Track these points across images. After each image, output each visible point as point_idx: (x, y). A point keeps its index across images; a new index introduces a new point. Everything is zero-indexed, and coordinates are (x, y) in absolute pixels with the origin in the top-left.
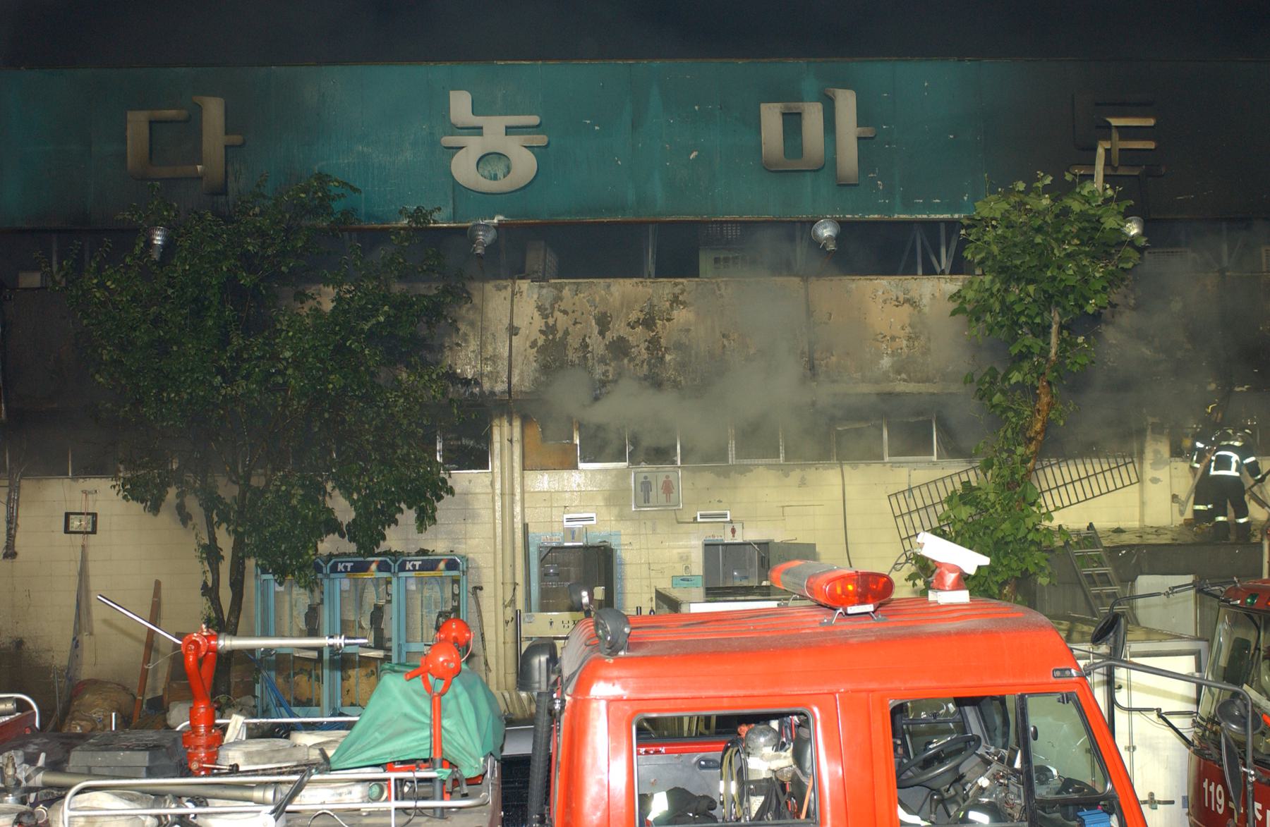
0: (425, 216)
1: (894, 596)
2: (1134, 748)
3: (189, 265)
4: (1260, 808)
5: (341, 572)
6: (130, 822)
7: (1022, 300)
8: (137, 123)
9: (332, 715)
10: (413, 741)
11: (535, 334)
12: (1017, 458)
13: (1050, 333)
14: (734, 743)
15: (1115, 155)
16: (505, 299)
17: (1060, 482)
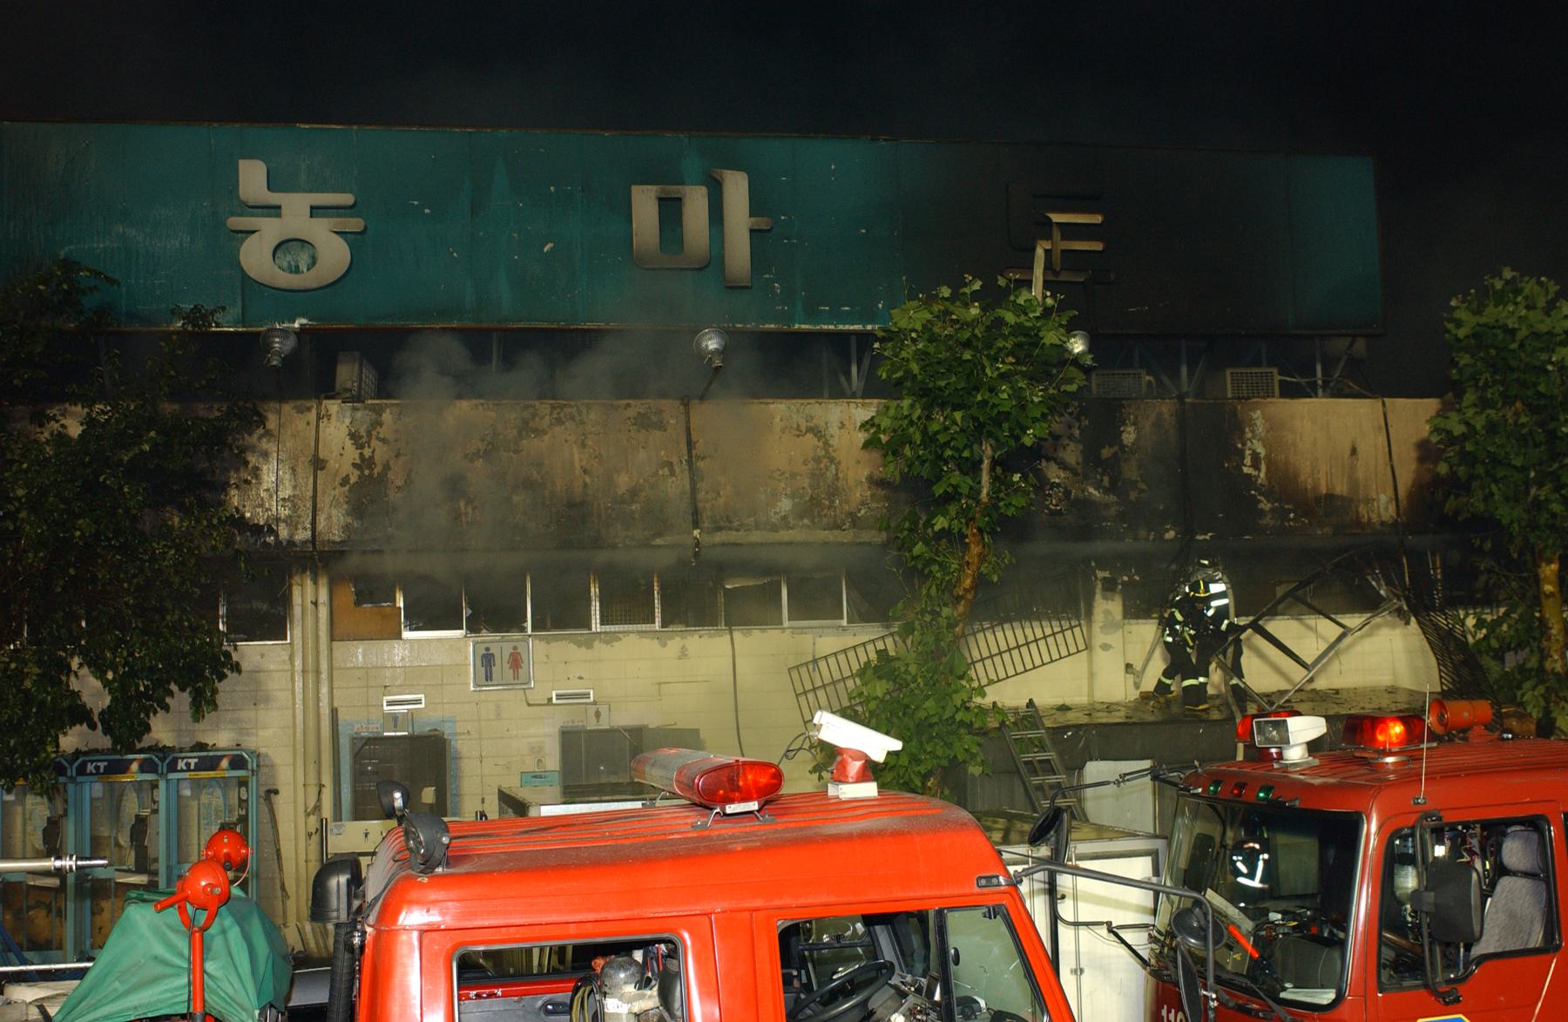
0: (204, 317)
1: (785, 790)
2: (1082, 971)
5: (91, 774)
7: (946, 429)
9: (79, 961)
10: (166, 991)
11: (346, 469)
12: (943, 622)
13: (981, 470)
14: (587, 981)
15: (1057, 258)
17: (1003, 647)
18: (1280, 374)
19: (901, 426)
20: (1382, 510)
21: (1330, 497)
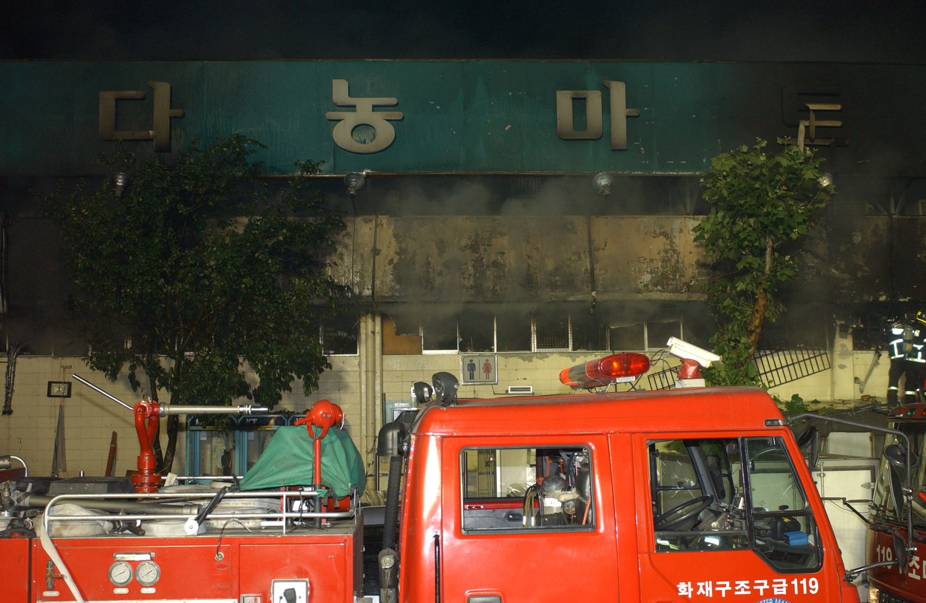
3: (142, 198)
4: (918, 560)
6: (93, 527)
8: (107, 99)
11: (392, 254)
13: (765, 254)
16: (370, 229)
17: (778, 366)
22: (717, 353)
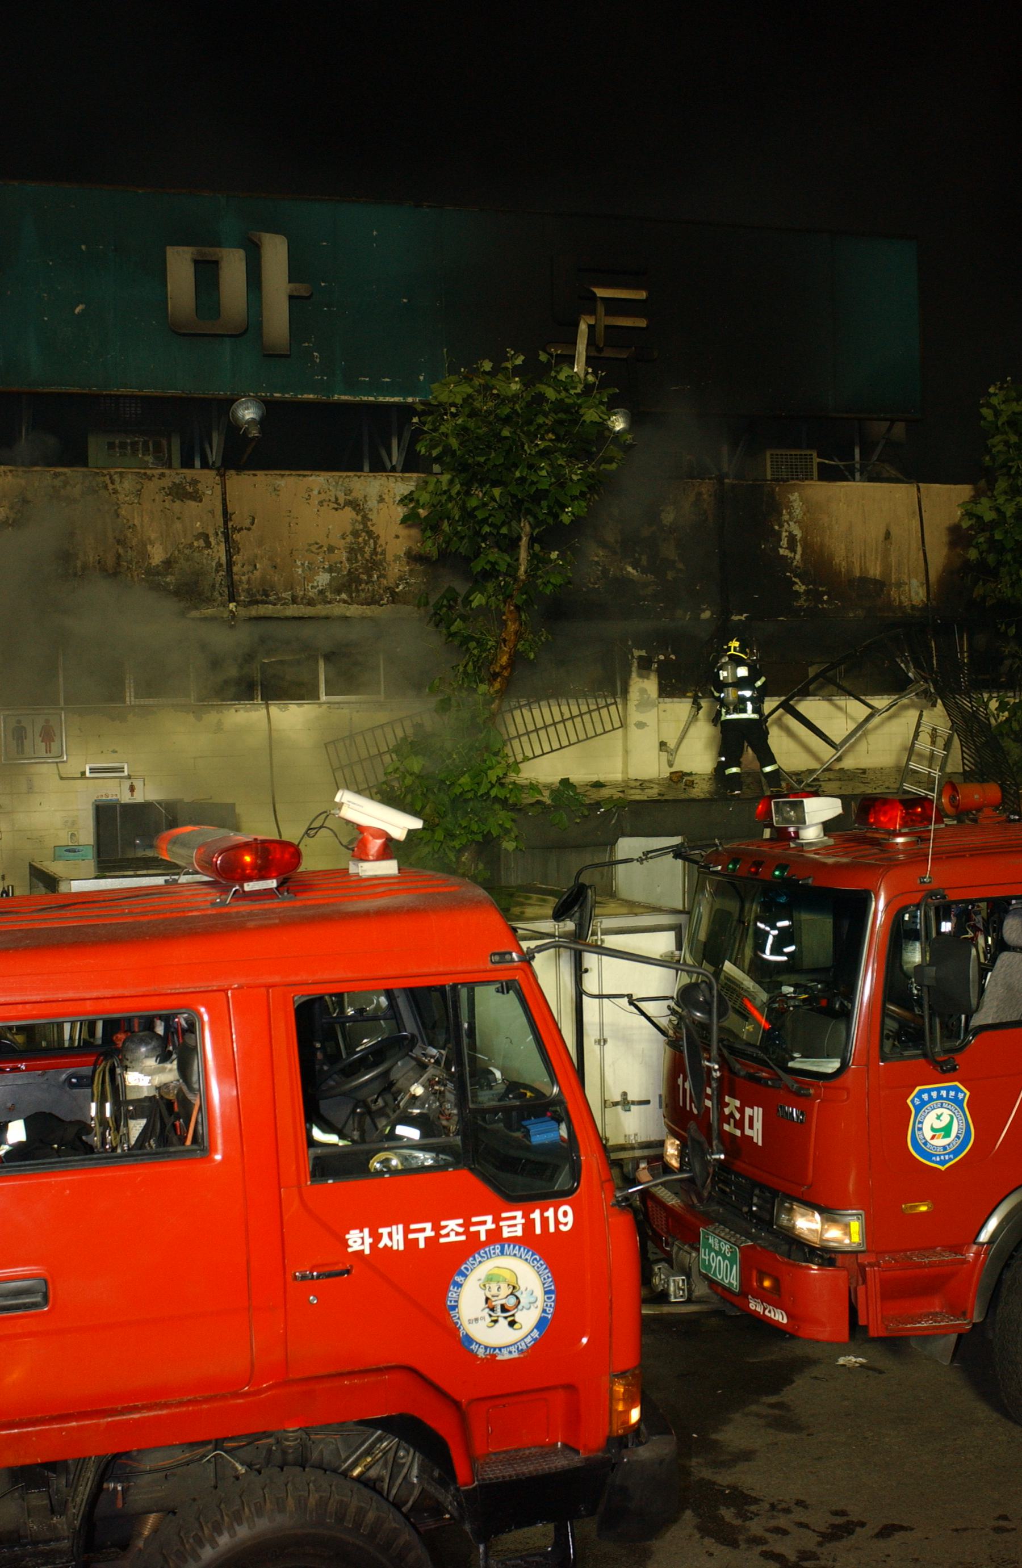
1: (301, 869)
2: (605, 1041)
7: (485, 505)
13: (519, 547)
15: (600, 332)
18: (819, 457)
19: (440, 501)
20: (913, 594)
21: (864, 580)
22: (416, 814)
